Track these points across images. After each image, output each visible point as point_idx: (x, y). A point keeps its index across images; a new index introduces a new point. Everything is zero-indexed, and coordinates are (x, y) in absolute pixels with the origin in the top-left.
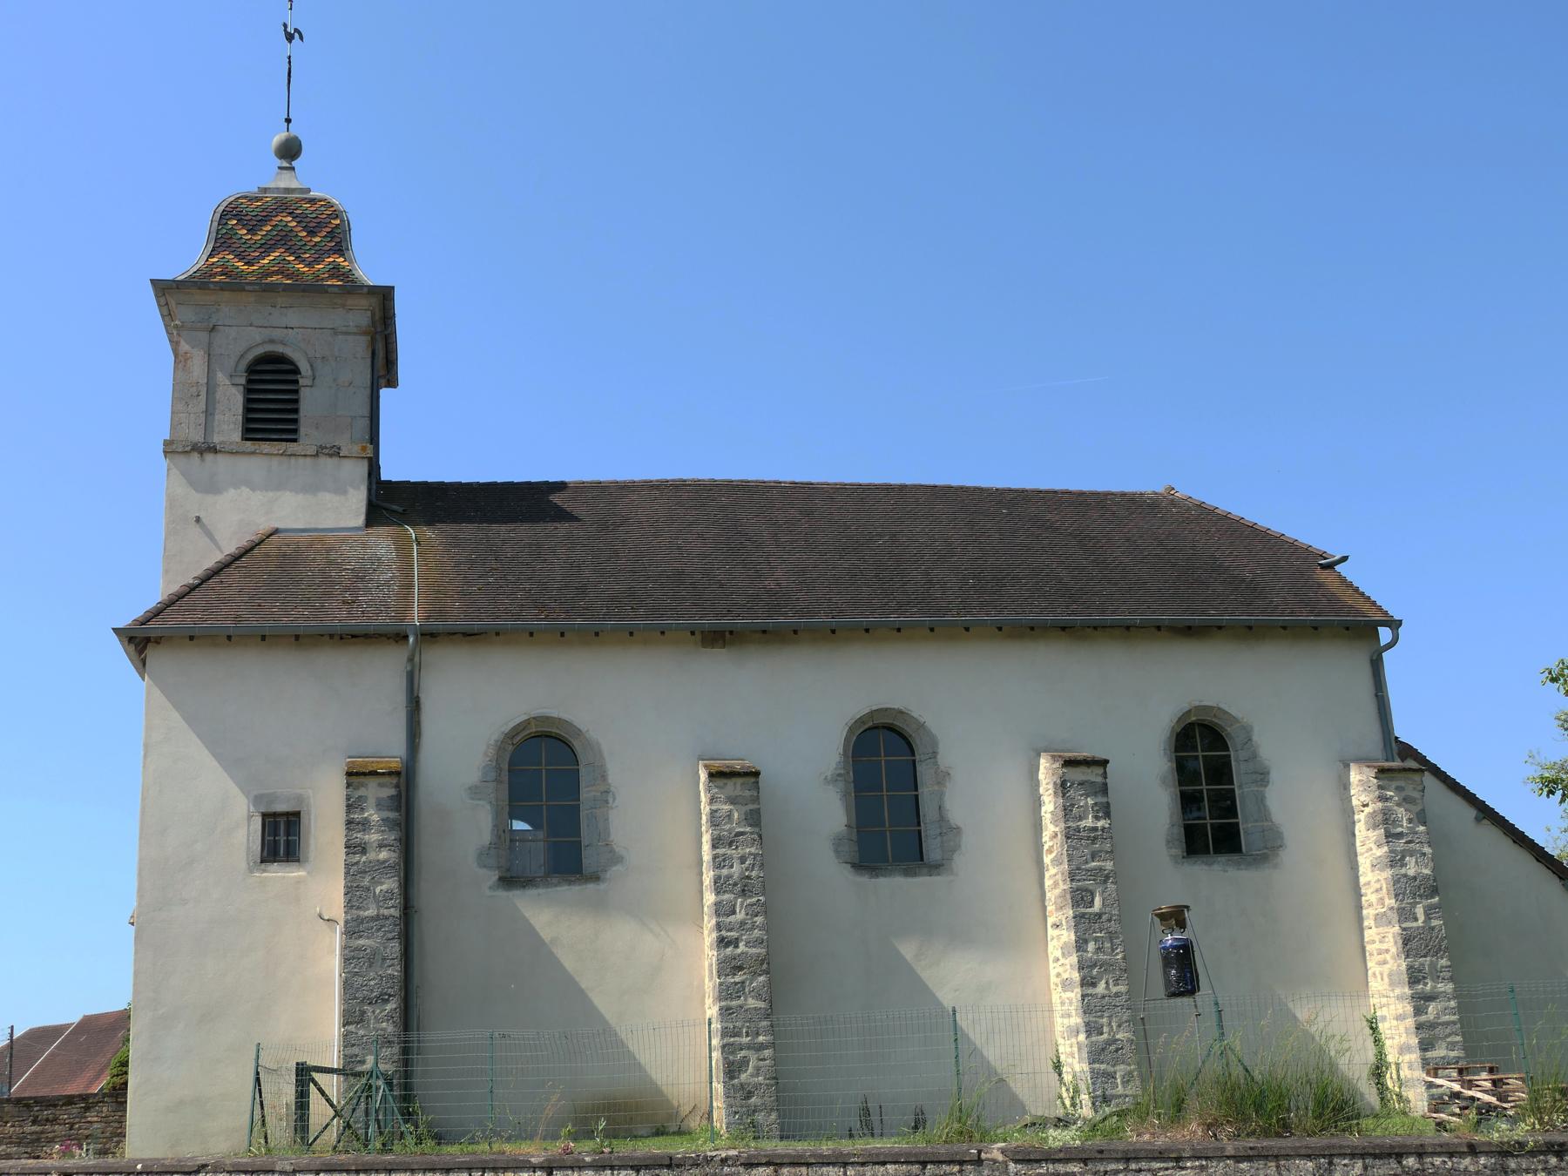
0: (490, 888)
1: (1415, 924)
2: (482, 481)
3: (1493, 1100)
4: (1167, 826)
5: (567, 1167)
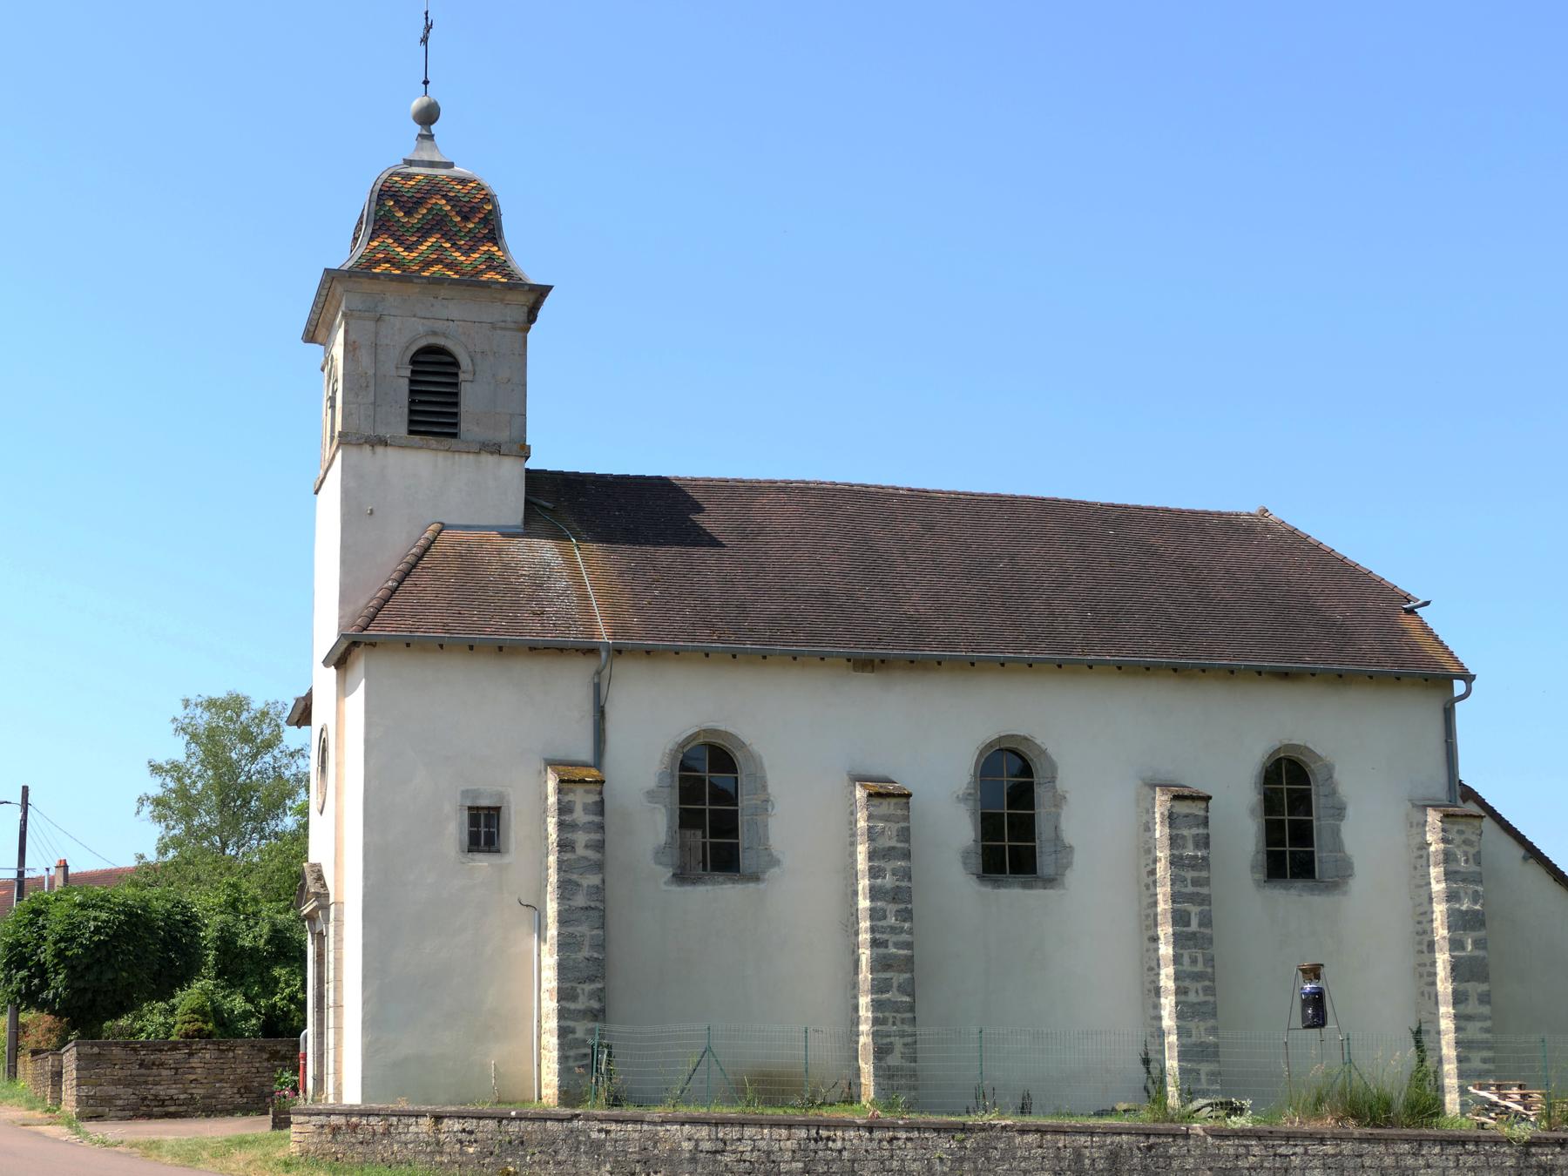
0: (665, 883)
1: (1463, 954)
2: (615, 473)
3: (1521, 1108)
4: (1252, 854)
5: (884, 1127)
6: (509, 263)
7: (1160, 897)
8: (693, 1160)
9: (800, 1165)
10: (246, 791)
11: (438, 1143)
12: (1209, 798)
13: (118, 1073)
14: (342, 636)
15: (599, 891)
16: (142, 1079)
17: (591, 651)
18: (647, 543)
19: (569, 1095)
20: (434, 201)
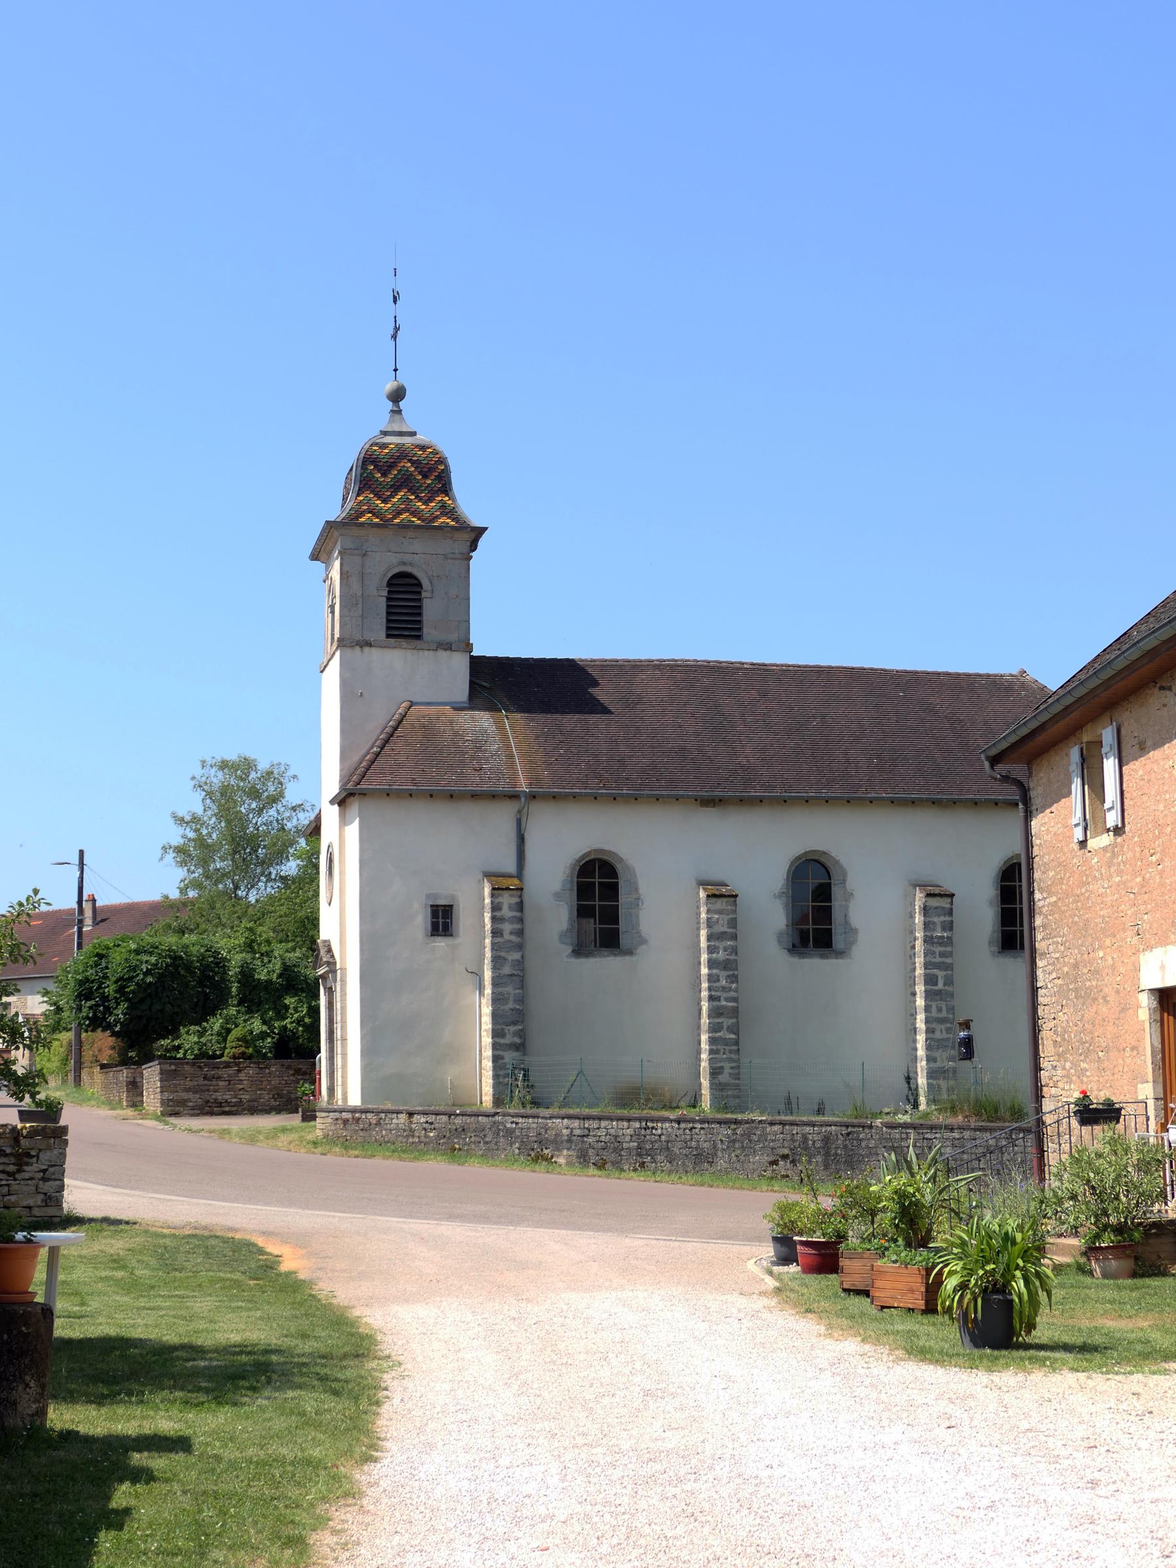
6: (457, 509)
7: (917, 965)
8: (569, 1141)
9: (636, 1144)
10: (253, 842)
11: (411, 1129)
12: (953, 895)
13: (189, 1084)
14: (343, 788)
15: (520, 964)
16: (207, 1087)
17: (514, 796)
18: (557, 712)
19: (498, 1101)
20: (402, 464)
